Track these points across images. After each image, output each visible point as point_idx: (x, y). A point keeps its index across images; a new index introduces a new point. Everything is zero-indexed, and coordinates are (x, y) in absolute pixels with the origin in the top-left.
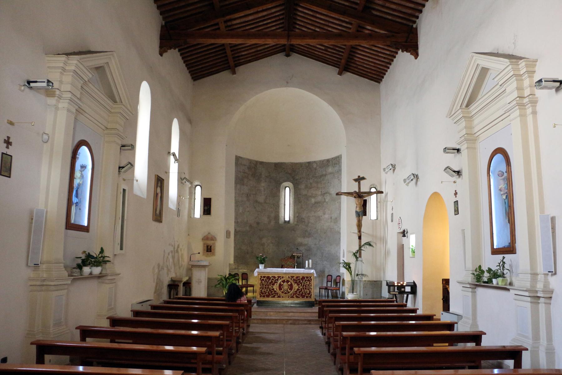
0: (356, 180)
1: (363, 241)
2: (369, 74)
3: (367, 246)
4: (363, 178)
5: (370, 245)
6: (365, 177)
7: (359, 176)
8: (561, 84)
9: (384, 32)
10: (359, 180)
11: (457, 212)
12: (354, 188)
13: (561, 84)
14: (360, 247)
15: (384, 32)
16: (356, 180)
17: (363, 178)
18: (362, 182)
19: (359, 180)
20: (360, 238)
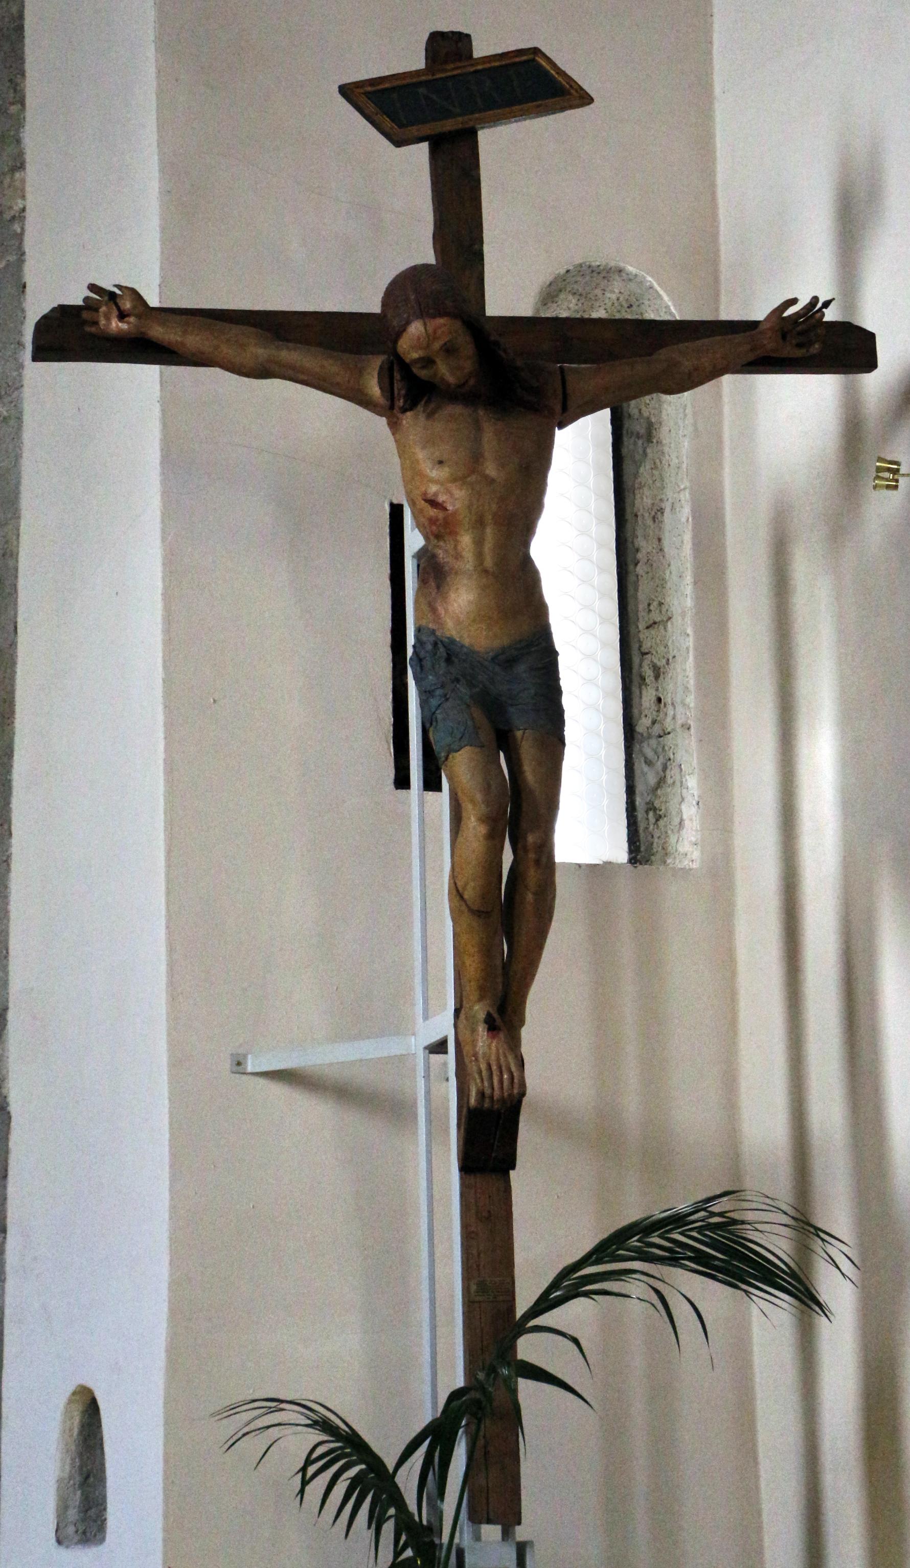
0: (387, 104)
1: (550, 1225)
2: (517, 60)
3: (686, 1283)
4: (533, 85)
5: (732, 1259)
6: (570, 59)
7: (447, 47)
8: (908, 475)
9: (438, 1450)
10: (451, 101)
11: (85, 1510)
12: (348, 228)
13: (908, 475)
14: (495, 1324)
15: (438, 1450)
16: (387, 104)
17: (533, 85)
18: (506, 149)
19: (451, 101)
20: (482, 1341)
